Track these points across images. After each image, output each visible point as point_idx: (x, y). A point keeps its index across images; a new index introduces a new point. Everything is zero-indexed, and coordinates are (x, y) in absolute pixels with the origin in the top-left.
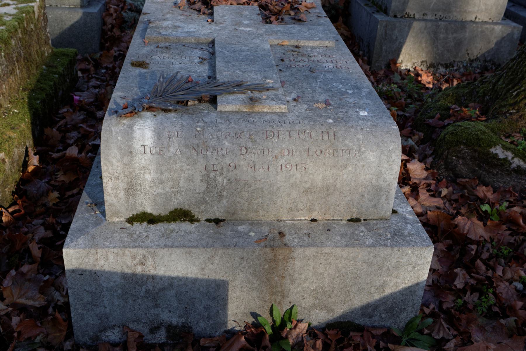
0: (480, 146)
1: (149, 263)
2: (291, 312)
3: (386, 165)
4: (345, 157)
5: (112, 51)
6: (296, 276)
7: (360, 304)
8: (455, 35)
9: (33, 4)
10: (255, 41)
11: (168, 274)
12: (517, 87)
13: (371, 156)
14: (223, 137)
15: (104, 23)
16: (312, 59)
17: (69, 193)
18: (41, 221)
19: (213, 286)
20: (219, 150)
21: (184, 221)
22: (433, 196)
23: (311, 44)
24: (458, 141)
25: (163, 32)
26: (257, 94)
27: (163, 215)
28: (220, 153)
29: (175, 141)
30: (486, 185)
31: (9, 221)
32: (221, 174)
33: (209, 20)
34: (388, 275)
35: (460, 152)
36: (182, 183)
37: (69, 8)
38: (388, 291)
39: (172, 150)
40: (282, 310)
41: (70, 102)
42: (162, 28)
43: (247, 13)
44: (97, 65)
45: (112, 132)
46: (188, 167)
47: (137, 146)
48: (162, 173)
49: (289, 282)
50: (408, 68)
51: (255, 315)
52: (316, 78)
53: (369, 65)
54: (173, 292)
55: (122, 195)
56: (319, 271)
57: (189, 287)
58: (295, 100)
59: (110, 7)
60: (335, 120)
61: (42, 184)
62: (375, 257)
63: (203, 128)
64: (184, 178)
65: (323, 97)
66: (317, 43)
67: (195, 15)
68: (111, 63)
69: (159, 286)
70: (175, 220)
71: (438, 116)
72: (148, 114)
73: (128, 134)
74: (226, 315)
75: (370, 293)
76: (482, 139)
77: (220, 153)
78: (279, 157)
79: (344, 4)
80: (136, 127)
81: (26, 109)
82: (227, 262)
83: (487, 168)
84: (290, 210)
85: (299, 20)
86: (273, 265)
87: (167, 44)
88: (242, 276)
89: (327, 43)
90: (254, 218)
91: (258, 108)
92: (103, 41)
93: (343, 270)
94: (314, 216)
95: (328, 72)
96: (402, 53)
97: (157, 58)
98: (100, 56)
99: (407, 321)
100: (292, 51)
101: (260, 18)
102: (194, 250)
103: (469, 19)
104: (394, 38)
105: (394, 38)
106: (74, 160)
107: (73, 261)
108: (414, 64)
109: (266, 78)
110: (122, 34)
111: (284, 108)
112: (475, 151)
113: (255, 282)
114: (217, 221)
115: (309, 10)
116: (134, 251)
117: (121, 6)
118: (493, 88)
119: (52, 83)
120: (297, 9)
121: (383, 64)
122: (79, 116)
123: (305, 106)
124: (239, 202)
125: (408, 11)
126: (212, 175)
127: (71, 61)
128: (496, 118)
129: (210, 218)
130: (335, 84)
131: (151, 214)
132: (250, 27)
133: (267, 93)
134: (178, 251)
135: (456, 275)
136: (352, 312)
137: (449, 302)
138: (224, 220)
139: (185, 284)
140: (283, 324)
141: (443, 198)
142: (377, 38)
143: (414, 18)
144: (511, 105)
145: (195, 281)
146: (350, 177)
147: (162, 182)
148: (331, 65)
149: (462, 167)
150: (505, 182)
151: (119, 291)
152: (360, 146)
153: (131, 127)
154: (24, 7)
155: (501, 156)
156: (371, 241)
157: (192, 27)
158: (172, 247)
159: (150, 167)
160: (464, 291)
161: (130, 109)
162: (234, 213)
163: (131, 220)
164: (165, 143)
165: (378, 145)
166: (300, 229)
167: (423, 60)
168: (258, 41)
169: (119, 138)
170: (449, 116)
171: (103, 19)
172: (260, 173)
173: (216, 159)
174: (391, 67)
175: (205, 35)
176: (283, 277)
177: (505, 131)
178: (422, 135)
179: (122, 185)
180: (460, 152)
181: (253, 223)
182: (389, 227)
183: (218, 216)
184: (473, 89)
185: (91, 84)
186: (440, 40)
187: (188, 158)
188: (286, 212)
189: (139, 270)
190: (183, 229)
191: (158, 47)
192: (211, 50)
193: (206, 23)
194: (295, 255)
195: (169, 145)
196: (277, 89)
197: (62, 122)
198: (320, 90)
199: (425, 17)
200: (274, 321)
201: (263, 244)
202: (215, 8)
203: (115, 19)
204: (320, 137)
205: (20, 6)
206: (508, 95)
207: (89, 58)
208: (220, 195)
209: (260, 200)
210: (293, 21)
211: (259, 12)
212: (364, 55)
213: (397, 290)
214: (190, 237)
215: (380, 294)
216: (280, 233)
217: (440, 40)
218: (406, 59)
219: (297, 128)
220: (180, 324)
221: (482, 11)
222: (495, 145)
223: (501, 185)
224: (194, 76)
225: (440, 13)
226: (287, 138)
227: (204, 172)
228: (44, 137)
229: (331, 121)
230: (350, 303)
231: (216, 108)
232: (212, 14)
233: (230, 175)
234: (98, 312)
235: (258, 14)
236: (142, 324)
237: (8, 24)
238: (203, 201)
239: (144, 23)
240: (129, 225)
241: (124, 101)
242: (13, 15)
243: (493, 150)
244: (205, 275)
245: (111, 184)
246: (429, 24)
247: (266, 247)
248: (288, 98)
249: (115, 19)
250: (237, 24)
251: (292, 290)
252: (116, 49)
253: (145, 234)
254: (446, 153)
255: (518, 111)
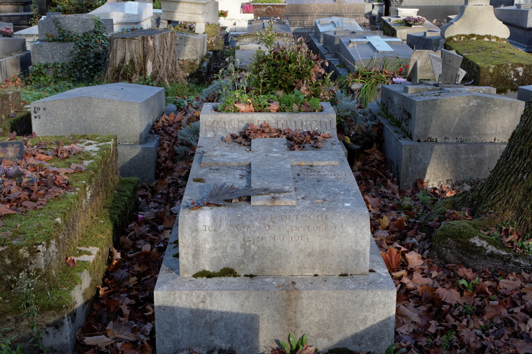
0: (462, 237)
1: (208, 302)
2: (303, 339)
3: (360, 236)
4: (333, 231)
5: (166, 180)
6: (304, 311)
7: (350, 333)
8: (475, 155)
9: (110, 143)
10: (280, 163)
11: (219, 309)
12: (494, 192)
13: (350, 230)
14: (254, 219)
15: (159, 157)
16: (320, 174)
17: (143, 279)
18: (126, 295)
19: (249, 318)
20: (252, 227)
21: (230, 276)
22: (425, 277)
23: (322, 164)
24: (445, 235)
25: (214, 159)
26: (277, 195)
27: (216, 272)
28: (252, 230)
29: (224, 223)
30: (468, 267)
31: (104, 295)
32: (253, 243)
33: (248, 150)
34: (368, 311)
35: (447, 243)
36: (229, 250)
37: (130, 145)
38: (369, 324)
39: (222, 228)
40: (296, 338)
41: (136, 218)
42: (213, 156)
43: (277, 143)
44: (154, 192)
45: (185, 218)
46: (233, 239)
47: (201, 226)
48: (216, 243)
49: (299, 316)
50: (435, 186)
51: (277, 342)
52: (320, 185)
53: (398, 185)
54: (222, 323)
55: (190, 258)
56: (320, 308)
57: (234, 319)
58: (303, 198)
59: (164, 143)
60: (327, 209)
61: (124, 273)
62: (356, 297)
63: (242, 215)
64: (230, 246)
65: (323, 196)
66: (327, 163)
67: (237, 146)
68: (166, 189)
69: (213, 319)
70: (224, 276)
71: (437, 218)
72: (207, 207)
73: (195, 220)
74: (258, 342)
75: (356, 325)
76: (463, 232)
77: (252, 230)
78: (290, 231)
79: (378, 131)
80: (200, 215)
81: (109, 220)
82: (258, 301)
83: (469, 255)
84: (299, 268)
85: (317, 147)
86: (288, 303)
87: (217, 167)
88: (268, 311)
89: (333, 163)
90: (276, 274)
91: (277, 203)
92: (157, 171)
93: (336, 307)
94: (316, 272)
95: (330, 181)
96: (427, 173)
97: (211, 176)
98: (156, 184)
99: (386, 349)
100: (307, 169)
101: (286, 146)
102: (237, 292)
103: (488, 140)
104: (419, 160)
105: (419, 160)
106: (147, 255)
107: (160, 299)
108: (440, 183)
109: (285, 186)
110: (174, 165)
111: (294, 202)
112: (459, 242)
113: (277, 316)
114: (251, 276)
115: (326, 140)
116: (198, 292)
117: (172, 141)
118: (479, 194)
119: (124, 203)
120: (316, 139)
121: (411, 184)
122: (145, 229)
123: (309, 202)
124: (265, 263)
125: (430, 135)
126: (247, 244)
127: (135, 187)
128: (480, 217)
129: (247, 274)
130: (333, 189)
131: (208, 272)
132: (277, 153)
133: (284, 194)
134: (226, 293)
135: (431, 324)
136: (346, 340)
137: (423, 341)
138: (256, 276)
139: (230, 317)
140: (298, 348)
141: (433, 279)
142: (403, 161)
143: (437, 141)
144: (489, 206)
145: (237, 315)
146: (337, 244)
147: (216, 249)
148: (333, 177)
149: (451, 256)
150: (483, 265)
151: (188, 322)
152: (342, 224)
153: (197, 215)
154: (104, 145)
155: (479, 244)
156: (353, 286)
157: (235, 155)
158: (222, 290)
159: (209, 239)
160: (435, 335)
161: (196, 205)
162: (263, 271)
163: (196, 276)
164: (218, 224)
165: (354, 222)
166: (306, 280)
167: (449, 179)
168: (282, 163)
169: (190, 221)
170: (445, 219)
171: (158, 153)
172: (278, 242)
173: (250, 233)
174: (417, 186)
175: (244, 160)
176: (295, 312)
177: (484, 227)
178: (424, 234)
179: (191, 252)
180: (447, 243)
181: (275, 277)
182: (367, 279)
183: (252, 272)
184: (465, 197)
185: (150, 206)
186: (462, 160)
187: (232, 233)
188: (297, 270)
189: (201, 306)
190: (229, 280)
191: (211, 169)
192: (248, 170)
193: (245, 152)
194: (303, 295)
195: (220, 225)
196: (291, 192)
197: (132, 233)
198: (321, 192)
199: (447, 141)
200: (291, 346)
201: (281, 288)
202: (252, 141)
203: (168, 153)
204: (316, 218)
205: (100, 144)
206: (488, 199)
207: (147, 186)
208: (253, 258)
209: (279, 261)
210: (312, 148)
211: (286, 142)
212: (394, 177)
213: (375, 323)
214: (233, 285)
215: (363, 326)
216: (292, 283)
217: (462, 160)
218: (432, 178)
219: (302, 213)
220: (227, 349)
221: (500, 133)
222: (473, 236)
223: (481, 268)
224: (236, 186)
225: (461, 137)
226: (295, 220)
227: (243, 242)
228: (120, 243)
229: (324, 209)
230: (343, 333)
231: (250, 204)
232: (250, 145)
233: (259, 244)
234: (173, 339)
235: (285, 144)
236: (202, 348)
237: (96, 158)
238: (242, 262)
239: (200, 153)
240: (194, 279)
241: (191, 201)
242: (97, 151)
243: (472, 240)
244: (243, 310)
245: (184, 251)
246: (450, 147)
247: (283, 290)
248: (298, 197)
249: (168, 153)
250: (268, 152)
251: (302, 323)
252: (169, 177)
253: (205, 283)
254: (437, 245)
255: (495, 210)
